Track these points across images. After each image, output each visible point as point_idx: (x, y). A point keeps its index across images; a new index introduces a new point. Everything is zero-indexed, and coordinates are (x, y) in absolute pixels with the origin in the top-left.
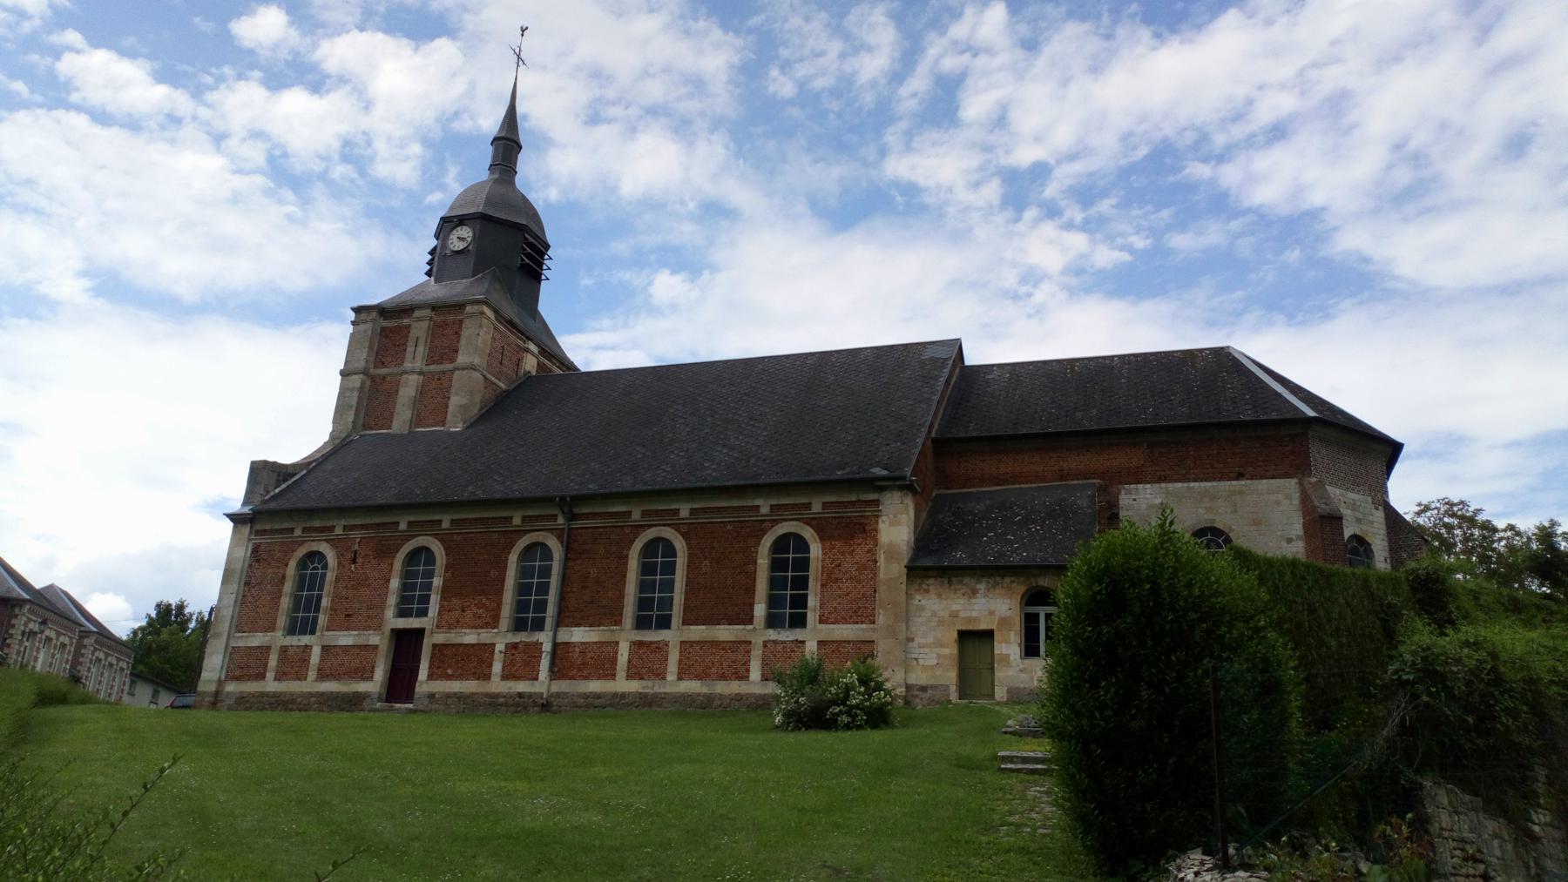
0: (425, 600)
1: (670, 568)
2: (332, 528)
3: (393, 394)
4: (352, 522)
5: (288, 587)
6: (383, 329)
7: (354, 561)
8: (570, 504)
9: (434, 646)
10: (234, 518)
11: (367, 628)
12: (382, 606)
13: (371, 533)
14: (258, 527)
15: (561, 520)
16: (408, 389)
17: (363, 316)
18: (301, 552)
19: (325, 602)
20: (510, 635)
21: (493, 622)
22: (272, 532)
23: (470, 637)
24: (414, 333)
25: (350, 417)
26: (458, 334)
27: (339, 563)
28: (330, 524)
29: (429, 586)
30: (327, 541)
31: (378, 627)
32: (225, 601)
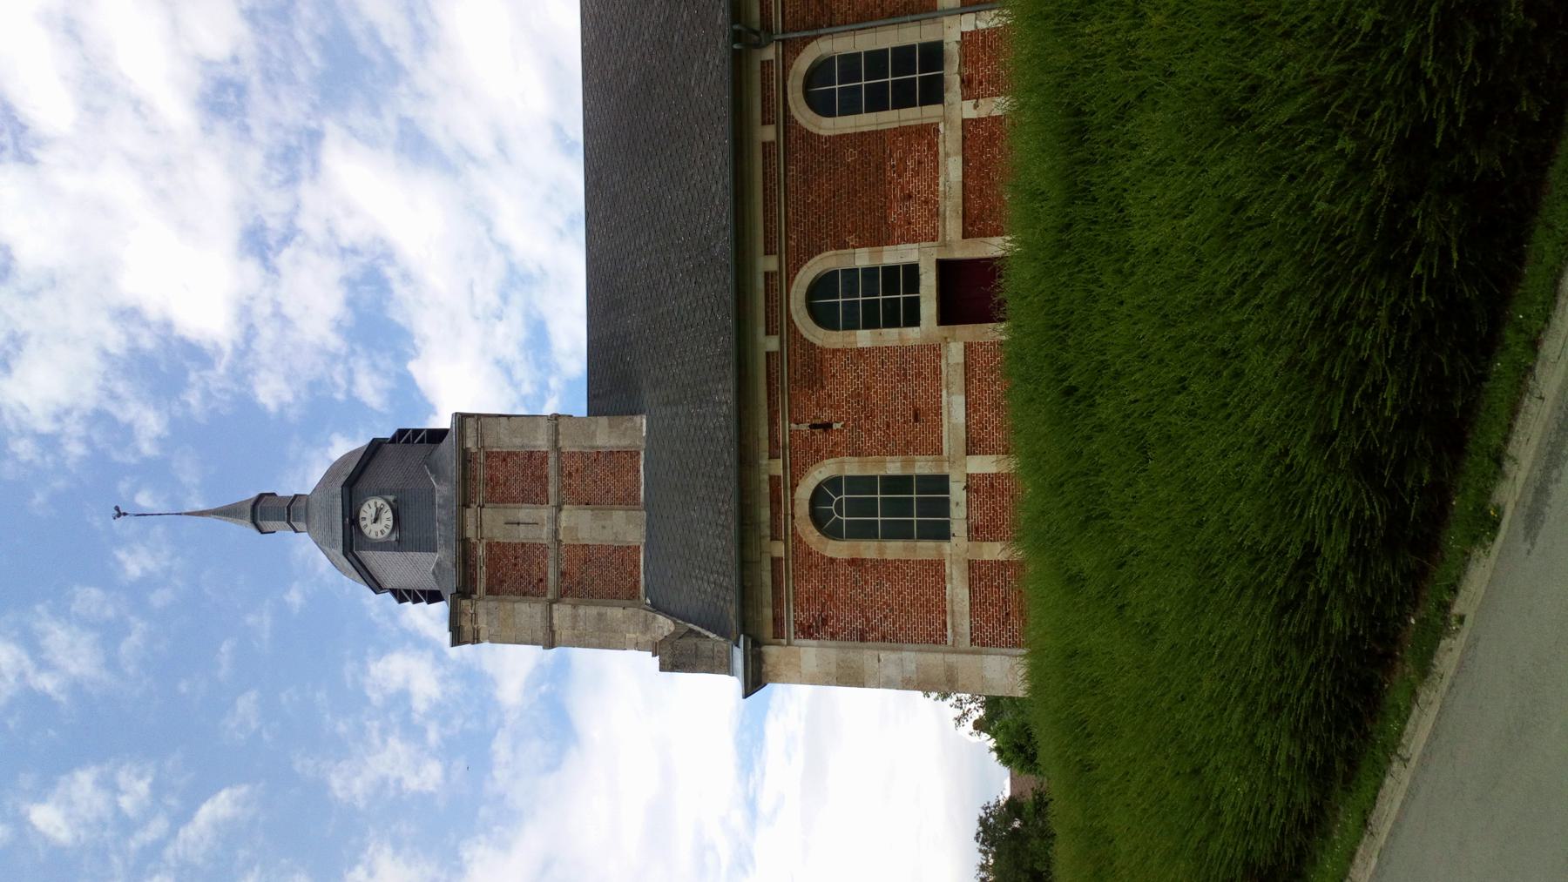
0: (891, 271)
1: (850, 64)
2: (774, 480)
3: (587, 554)
5: (868, 549)
6: (490, 591)
7: (827, 427)
8: (744, 40)
10: (754, 682)
11: (937, 372)
12: (903, 351)
14: (768, 631)
15: (770, 53)
17: (467, 626)
18: (811, 535)
20: (948, 97)
21: (928, 133)
22: (777, 603)
23: (952, 170)
24: (500, 534)
25: (616, 613)
26: (506, 457)
27: (832, 454)
29: (870, 272)
30: (794, 487)
31: (935, 350)
32: (892, 671)
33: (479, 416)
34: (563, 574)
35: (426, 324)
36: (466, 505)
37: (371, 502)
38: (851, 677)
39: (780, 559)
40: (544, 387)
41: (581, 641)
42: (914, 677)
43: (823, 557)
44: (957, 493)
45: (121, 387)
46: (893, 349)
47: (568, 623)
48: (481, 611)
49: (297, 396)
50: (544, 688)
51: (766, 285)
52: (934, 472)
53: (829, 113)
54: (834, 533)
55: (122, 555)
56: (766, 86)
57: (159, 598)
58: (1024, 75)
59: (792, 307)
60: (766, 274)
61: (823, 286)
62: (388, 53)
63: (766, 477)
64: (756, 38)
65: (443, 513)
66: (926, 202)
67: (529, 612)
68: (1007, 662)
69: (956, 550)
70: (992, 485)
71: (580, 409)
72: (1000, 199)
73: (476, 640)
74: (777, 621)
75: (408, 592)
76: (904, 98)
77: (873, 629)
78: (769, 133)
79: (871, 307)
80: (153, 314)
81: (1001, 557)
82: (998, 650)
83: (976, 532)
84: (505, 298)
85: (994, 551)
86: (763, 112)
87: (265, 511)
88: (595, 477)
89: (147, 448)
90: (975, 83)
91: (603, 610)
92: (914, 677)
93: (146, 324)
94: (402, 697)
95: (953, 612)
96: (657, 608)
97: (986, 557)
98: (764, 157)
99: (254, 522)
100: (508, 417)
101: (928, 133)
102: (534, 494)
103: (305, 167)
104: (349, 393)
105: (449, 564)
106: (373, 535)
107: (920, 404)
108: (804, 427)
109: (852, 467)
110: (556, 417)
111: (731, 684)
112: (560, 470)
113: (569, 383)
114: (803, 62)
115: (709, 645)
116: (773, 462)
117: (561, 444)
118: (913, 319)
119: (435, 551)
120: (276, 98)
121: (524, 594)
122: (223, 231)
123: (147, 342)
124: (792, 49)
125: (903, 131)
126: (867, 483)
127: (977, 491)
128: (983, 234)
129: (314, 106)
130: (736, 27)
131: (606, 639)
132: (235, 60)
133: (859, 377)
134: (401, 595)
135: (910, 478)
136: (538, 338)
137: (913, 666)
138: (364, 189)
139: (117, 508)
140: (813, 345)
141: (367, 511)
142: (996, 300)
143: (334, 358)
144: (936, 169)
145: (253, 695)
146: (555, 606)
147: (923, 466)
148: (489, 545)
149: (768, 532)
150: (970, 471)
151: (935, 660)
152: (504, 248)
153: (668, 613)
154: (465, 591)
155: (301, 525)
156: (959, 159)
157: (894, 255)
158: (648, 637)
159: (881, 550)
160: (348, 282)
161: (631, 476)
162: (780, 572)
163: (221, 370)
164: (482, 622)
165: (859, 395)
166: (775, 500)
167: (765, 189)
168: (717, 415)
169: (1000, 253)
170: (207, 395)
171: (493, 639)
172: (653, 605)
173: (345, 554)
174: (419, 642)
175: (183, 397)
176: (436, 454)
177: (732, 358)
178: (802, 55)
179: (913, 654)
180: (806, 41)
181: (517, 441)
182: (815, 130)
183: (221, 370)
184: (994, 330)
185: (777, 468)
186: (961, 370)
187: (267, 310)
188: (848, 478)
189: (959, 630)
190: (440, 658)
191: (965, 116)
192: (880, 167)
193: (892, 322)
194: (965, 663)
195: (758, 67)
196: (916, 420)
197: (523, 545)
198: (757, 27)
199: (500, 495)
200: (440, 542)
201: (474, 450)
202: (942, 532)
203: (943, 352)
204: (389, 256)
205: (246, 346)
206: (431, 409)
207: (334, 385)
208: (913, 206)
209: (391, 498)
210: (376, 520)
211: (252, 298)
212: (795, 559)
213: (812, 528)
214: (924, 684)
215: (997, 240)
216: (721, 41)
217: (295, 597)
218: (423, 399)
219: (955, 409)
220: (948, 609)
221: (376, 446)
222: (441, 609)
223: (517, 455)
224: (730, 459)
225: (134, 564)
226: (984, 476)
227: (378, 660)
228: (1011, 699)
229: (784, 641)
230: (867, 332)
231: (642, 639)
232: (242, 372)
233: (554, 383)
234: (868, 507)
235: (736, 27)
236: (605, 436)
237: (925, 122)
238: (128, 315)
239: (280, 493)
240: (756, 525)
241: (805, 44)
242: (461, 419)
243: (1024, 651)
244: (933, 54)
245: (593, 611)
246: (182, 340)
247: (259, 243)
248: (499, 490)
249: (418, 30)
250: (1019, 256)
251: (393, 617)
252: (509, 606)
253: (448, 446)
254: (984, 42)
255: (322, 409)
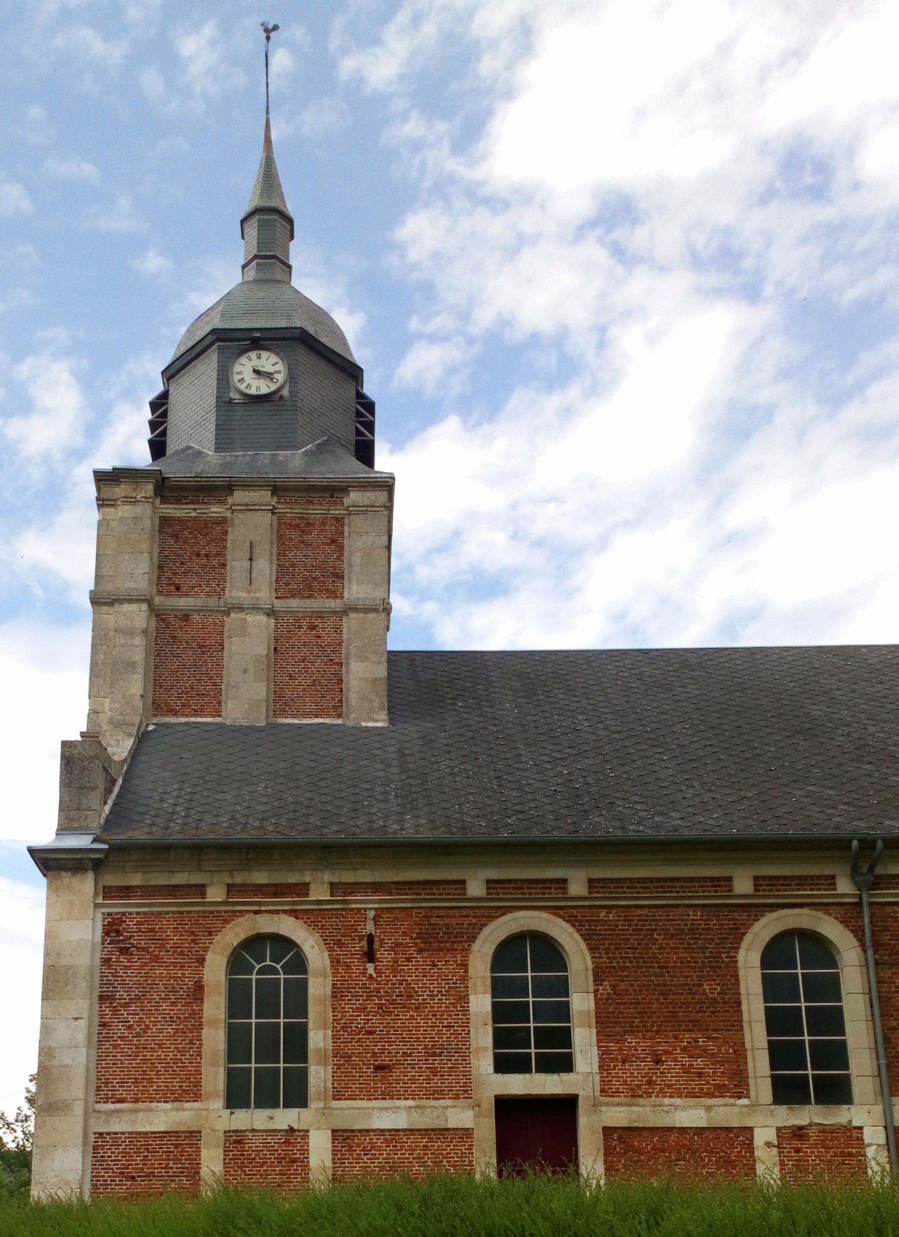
0: (564, 1038)
2: (302, 889)
3: (211, 647)
4: (348, 877)
5: (215, 1007)
7: (370, 956)
9: (608, 1131)
10: (48, 861)
11: (437, 1094)
13: (403, 901)
14: (112, 880)
15: (844, 887)
16: (248, 643)
17: (120, 490)
18: (233, 935)
19: (318, 1039)
20: (782, 1110)
21: (736, 1084)
22: (148, 891)
23: (689, 1115)
25: (136, 685)
26: (337, 543)
27: (335, 962)
28: (293, 878)
29: (563, 1012)
30: (294, 914)
31: (464, 1091)
33: (390, 508)
34: (186, 617)
35: (503, 443)
36: (276, 490)
37: (280, 367)
38: (55, 982)
39: (203, 895)
40: (424, 595)
41: (101, 640)
42: (55, 1063)
43: (206, 950)
44: (285, 1118)
45: (429, 29)
46: (466, 1040)
47: (123, 623)
48: (138, 510)
49: (414, 267)
50: (39, 592)
51: (551, 881)
52: (312, 1090)
53: (766, 962)
54: (236, 963)
55: (208, 30)
56: (802, 881)
57: (151, 80)
58: (807, 1202)
59: (522, 913)
60: (564, 881)
61: (548, 952)
62: (859, 389)
63: (307, 878)
64: (865, 869)
65: (265, 461)
66: (649, 1083)
67: (138, 572)
68: (74, 1177)
69: (213, 1116)
70: (294, 1161)
71: (397, 642)
72: (653, 1173)
73: (102, 503)
74: (125, 892)
75: (164, 415)
76: (781, 1055)
77: (115, 1011)
78: (743, 885)
79: (521, 1012)
80: (530, 73)
81: (204, 1171)
82: (89, 1166)
83: (235, 1140)
84: (539, 543)
85: (212, 1162)
86: (771, 878)
87: (270, 225)
88: (308, 657)
89: (348, 65)
90: (797, 1144)
91: (140, 670)
92: (55, 1063)
93: (510, 66)
94: (22, 404)
95: (136, 1111)
96: (142, 738)
97: (204, 1153)
98: (712, 879)
99: (256, 257)
100: (389, 547)
101: (736, 1084)
102: (288, 582)
103: (713, 279)
104: (419, 336)
105: (199, 467)
106: (237, 368)
107: (396, 1073)
108: (370, 927)
109: (318, 987)
110: (387, 610)
111: (46, 835)
112: (320, 615)
113: (427, 629)
114: (831, 929)
115: (95, 803)
116: (326, 888)
117: (353, 615)
118: (503, 1065)
119: (217, 450)
120: (803, 240)
121: (160, 567)
122: (629, 167)
123: (488, 65)
124: (849, 915)
125: (740, 1053)
126: (298, 1002)
127: (287, 1142)
128: (608, 1152)
129: (791, 292)
130: (880, 844)
131: (104, 672)
132: (857, 186)
133: (432, 997)
134: (160, 405)
135: (305, 1059)
136: (488, 586)
137: (67, 1061)
138: (683, 352)
139: (276, 28)
140: (473, 939)
141: (269, 361)
142: (526, 1166)
143: (465, 317)
144: (692, 1095)
145: (26, 206)
146: (145, 606)
147: (319, 1076)
148: (224, 520)
149: (238, 879)
150: (312, 1134)
151: (76, 1087)
152: (603, 543)
153: (135, 753)
154: (165, 488)
155: (251, 273)
156: (703, 1123)
157: (584, 1041)
158: (105, 727)
159: (214, 1023)
160: (562, 337)
161: (310, 706)
162: (188, 895)
163: (452, 165)
164: (124, 511)
165: (410, 997)
166: (278, 890)
167: (672, 880)
168: (387, 817)
169: (583, 1171)
170: (417, 146)
171: (102, 525)
172: (146, 733)
173: (214, 331)
174: (95, 428)
175: (415, 114)
176: (340, 451)
177: (458, 837)
178: (840, 927)
179: (83, 1060)
180: (858, 932)
181: (357, 559)
182: (745, 943)
183: (452, 165)
184: (488, 1164)
185: (319, 893)
186: (439, 1124)
187: (527, 228)
188: (305, 982)
189: (114, 1119)
190: (77, 455)
191: (756, 1132)
192: (695, 1025)
193: (500, 1038)
194: (72, 1125)
195: (827, 872)
196: (378, 1068)
197: (224, 565)
198: (880, 870)
199: (287, 534)
200: (228, 456)
201: (346, 501)
202: (236, 1098)
203: (461, 1102)
204: (595, 391)
205: (479, 198)
206: (398, 446)
207: (428, 317)
208: (646, 1066)
209: (285, 392)
210: (257, 373)
211: (542, 207)
212: (204, 915)
213: (243, 936)
214: (46, 1075)
215: (600, 1168)
216: (862, 824)
217: (154, 262)
218: (411, 435)
219: (389, 1116)
220: (140, 1105)
221: (352, 373)
222: (140, 455)
223: (340, 557)
224: (332, 833)
225: (196, 47)
226: (305, 1151)
227: (72, 373)
228: (28, 1183)
229: (100, 900)
230: (489, 1008)
231: (103, 719)
232: (444, 191)
233: (430, 608)
234: (268, 1008)
235: (880, 844)
236: (362, 674)
237: (751, 1082)
238: (524, 36)
239: (294, 246)
240: (247, 867)
241: (854, 932)
242: (387, 485)
243: (87, 1198)
244: (836, 1091)
245: (138, 655)
246: (489, 113)
247: (615, 217)
248: (295, 535)
249: (887, 431)
250: (580, 1195)
251: (129, 393)
252: (145, 546)
253: (352, 467)
254: (850, 1155)
255: (400, 298)
